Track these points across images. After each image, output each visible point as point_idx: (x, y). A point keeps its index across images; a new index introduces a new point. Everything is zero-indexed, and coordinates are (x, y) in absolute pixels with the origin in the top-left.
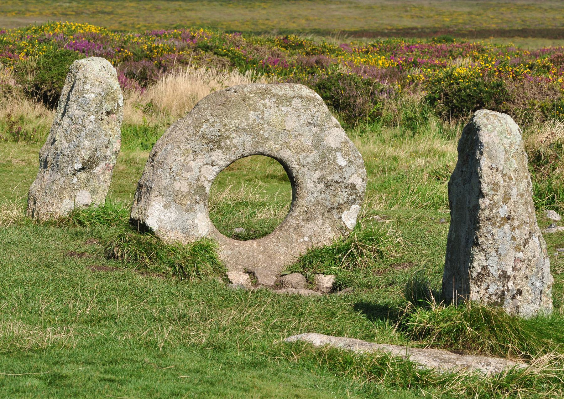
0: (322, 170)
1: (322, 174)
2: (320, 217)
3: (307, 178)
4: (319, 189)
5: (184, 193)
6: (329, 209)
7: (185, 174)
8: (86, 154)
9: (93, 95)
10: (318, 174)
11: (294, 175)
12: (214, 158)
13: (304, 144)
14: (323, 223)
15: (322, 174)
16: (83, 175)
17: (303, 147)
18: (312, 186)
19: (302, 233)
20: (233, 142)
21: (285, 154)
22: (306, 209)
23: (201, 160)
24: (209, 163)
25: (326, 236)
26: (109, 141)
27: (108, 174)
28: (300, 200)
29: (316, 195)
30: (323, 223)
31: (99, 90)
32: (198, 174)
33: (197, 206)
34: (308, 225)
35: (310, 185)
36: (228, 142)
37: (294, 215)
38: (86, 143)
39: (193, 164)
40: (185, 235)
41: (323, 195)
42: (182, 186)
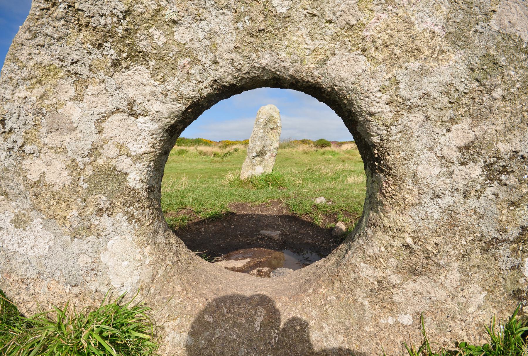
0: (477, 118)
1: (478, 131)
2: (456, 265)
3: (418, 146)
4: (461, 183)
5: (56, 188)
6: (489, 244)
7: (52, 139)
8: (258, 149)
9: (262, 120)
10: (461, 133)
11: (376, 139)
12: (132, 92)
13: (417, 29)
14: (464, 283)
15: (478, 131)
16: (258, 159)
17: (414, 38)
18: (436, 171)
19: (392, 303)
20: (177, 36)
21: (343, 70)
22: (409, 241)
23: (100, 100)
24: (122, 107)
25: (469, 319)
26: (272, 143)
27: (273, 159)
28: (392, 213)
29: (447, 201)
30: (464, 283)
31: (265, 117)
32: (94, 138)
33: (106, 221)
34: (411, 284)
35: (429, 170)
36: (159, 36)
37: (370, 252)
38: (259, 143)
39: (74, 112)
40: (76, 290)
41: (472, 203)
42: (56, 174)
